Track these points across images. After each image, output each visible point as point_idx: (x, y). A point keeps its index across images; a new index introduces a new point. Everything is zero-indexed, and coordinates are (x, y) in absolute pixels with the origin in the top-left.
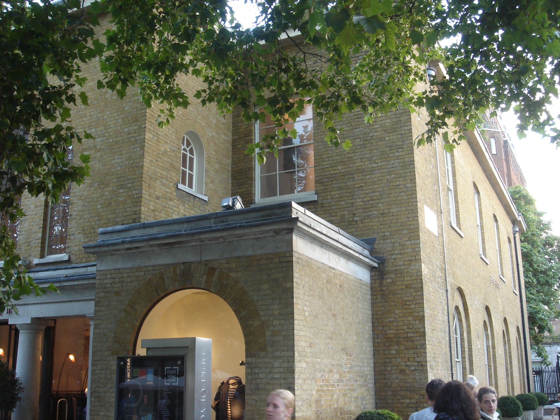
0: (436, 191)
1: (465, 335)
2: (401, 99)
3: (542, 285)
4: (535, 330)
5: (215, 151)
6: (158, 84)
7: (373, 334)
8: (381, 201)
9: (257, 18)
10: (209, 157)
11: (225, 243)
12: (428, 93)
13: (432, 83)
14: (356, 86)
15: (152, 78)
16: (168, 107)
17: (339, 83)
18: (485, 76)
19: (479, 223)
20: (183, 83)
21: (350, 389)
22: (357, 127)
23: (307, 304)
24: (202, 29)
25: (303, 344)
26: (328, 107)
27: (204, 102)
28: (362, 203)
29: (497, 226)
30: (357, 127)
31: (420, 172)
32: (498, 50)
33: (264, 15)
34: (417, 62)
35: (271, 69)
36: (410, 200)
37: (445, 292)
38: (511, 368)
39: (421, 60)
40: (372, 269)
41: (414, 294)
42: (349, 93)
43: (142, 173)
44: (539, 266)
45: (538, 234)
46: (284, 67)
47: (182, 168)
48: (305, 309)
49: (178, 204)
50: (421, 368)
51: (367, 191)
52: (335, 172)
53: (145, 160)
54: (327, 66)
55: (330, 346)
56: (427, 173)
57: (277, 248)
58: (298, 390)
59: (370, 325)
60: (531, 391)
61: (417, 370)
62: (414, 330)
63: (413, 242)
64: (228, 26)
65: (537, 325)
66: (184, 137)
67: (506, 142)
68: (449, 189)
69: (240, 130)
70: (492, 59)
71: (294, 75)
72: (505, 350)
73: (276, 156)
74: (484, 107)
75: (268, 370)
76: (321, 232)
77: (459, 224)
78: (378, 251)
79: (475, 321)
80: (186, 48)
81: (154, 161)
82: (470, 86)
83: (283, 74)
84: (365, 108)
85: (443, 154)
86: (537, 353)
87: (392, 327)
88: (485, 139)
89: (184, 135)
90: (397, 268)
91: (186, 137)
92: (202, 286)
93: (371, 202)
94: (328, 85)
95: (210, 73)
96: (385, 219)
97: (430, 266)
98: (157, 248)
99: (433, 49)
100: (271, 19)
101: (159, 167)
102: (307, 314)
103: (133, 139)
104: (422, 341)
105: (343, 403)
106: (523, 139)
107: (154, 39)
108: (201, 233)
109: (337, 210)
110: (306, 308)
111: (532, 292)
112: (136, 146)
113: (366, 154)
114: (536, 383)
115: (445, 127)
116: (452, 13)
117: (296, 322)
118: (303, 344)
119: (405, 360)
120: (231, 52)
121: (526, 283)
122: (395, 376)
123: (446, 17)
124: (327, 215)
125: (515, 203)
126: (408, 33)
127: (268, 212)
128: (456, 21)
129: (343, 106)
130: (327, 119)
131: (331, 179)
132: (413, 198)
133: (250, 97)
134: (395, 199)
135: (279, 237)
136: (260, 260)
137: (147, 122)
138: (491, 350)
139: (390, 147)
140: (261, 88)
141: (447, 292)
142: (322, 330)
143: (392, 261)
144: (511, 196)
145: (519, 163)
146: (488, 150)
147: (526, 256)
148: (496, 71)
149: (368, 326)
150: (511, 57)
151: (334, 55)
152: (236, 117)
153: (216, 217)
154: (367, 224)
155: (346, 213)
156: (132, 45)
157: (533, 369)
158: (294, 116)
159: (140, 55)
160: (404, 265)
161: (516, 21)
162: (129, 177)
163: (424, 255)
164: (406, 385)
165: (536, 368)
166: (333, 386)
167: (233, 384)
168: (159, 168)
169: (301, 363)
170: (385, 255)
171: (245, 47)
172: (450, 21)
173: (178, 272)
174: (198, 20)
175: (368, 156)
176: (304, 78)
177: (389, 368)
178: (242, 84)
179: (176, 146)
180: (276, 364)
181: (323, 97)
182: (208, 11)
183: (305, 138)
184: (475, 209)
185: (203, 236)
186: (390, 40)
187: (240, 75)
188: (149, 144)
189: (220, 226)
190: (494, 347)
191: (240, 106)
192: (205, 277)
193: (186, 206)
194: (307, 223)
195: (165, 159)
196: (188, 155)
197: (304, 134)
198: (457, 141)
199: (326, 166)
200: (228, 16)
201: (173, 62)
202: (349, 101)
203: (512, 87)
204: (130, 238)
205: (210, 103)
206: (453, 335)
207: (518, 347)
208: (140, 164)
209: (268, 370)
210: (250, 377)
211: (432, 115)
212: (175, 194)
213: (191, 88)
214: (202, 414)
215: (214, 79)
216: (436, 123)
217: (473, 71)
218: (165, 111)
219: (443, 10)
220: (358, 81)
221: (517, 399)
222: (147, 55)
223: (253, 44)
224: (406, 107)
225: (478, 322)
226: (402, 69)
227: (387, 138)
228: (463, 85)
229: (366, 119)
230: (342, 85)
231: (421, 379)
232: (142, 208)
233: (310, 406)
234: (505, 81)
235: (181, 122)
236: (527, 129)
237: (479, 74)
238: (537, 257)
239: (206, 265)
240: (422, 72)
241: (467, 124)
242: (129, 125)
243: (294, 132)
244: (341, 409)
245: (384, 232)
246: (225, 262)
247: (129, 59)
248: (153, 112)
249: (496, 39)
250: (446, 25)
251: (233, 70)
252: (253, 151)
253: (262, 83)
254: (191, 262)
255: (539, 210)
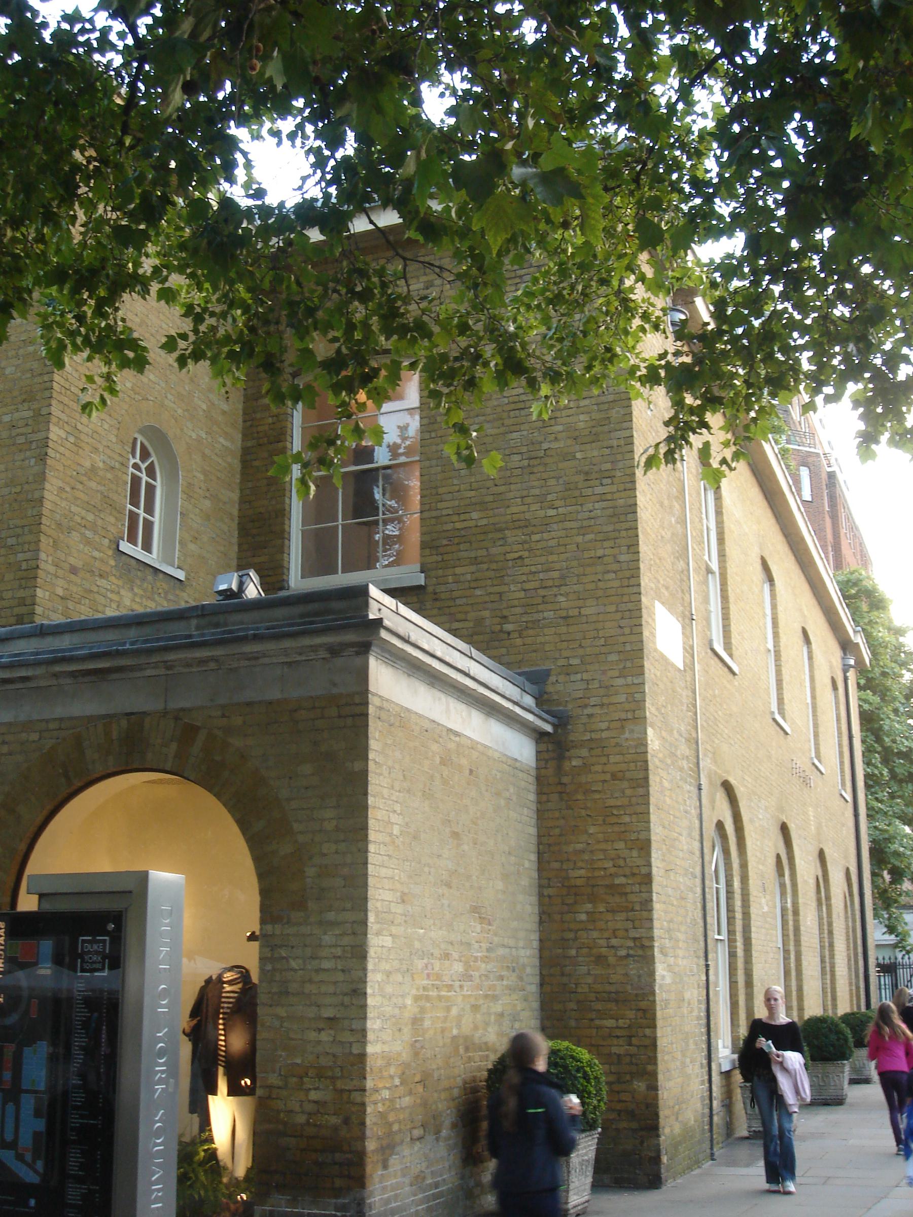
0: (682, 572)
1: (737, 884)
2: (612, 370)
3: (901, 781)
4: (883, 877)
5: (205, 473)
6: (80, 318)
7: (540, 878)
8: (564, 589)
9: (304, 179)
10: (190, 485)
11: (220, 671)
12: (670, 357)
13: (679, 336)
14: (514, 337)
15: (68, 304)
16: (105, 370)
17: (479, 327)
18: (793, 325)
19: (770, 645)
20: (137, 320)
21: (486, 996)
22: (513, 428)
23: (398, 808)
24: (181, 200)
25: (387, 896)
26: (453, 378)
27: (182, 361)
28: (522, 594)
29: (810, 653)
30: (513, 428)
31: (649, 531)
32: (821, 271)
33: (319, 173)
34: (648, 289)
35: (330, 292)
36: (626, 590)
37: (696, 791)
38: (832, 956)
39: (656, 286)
40: (540, 736)
41: (628, 792)
42: (500, 350)
43: (40, 515)
44: (894, 741)
45: (894, 673)
46: (359, 289)
47: (129, 506)
48: (393, 820)
49: (118, 586)
50: (640, 952)
51: (533, 569)
52: (465, 524)
53: (47, 486)
54: (450, 292)
55: (446, 902)
56: (664, 534)
57: (335, 685)
58: (373, 995)
59: (534, 857)
60: (873, 1007)
61: (632, 956)
62: (627, 871)
63: (629, 679)
64: (237, 193)
65: (889, 866)
66: (135, 439)
67: (832, 476)
68: (709, 571)
69: (260, 428)
70: (808, 289)
71: (380, 305)
72: (820, 918)
73: (338, 482)
74: (789, 390)
75: (308, 951)
76: (431, 651)
77: (728, 646)
78: (555, 697)
79: (758, 854)
80: (145, 236)
81: (68, 489)
82: (760, 345)
83: (356, 303)
84: (533, 384)
85: (699, 494)
86: (886, 926)
87: (580, 864)
88: (788, 467)
89: (136, 435)
90: (594, 736)
91: (140, 438)
92: (168, 768)
93: (542, 592)
94: (455, 331)
95: (198, 297)
96: (572, 629)
97: (664, 734)
98: (69, 681)
99: (682, 265)
100: (335, 181)
101: (79, 502)
102: (396, 830)
103: (21, 440)
104: (644, 895)
105: (472, 1026)
106: (870, 462)
107: (74, 218)
108: (166, 649)
109: (468, 608)
110: (394, 818)
111: (880, 795)
112: (28, 453)
113: (533, 487)
114: (883, 991)
115: (704, 431)
116: (725, 188)
117: (372, 848)
118: (387, 896)
119: (606, 935)
120: (244, 252)
121: (867, 776)
122: (584, 969)
123: (714, 195)
124: (444, 618)
125: (847, 605)
126: (630, 227)
127: (315, 606)
128: (734, 204)
129: (485, 380)
130: (452, 405)
131: (456, 540)
132: (633, 586)
133: (283, 350)
134: (592, 586)
135: (339, 662)
136: (296, 710)
137: (54, 402)
138: (790, 917)
139: (587, 473)
140: (308, 332)
141: (700, 789)
142: (429, 865)
143: (584, 720)
144: (841, 590)
145: (857, 522)
146: (794, 490)
147: (869, 720)
148: (816, 315)
149: (530, 861)
150: (848, 286)
151: (469, 268)
152: (251, 399)
153: (203, 616)
154: (528, 641)
155: (486, 614)
156: (24, 230)
157: (877, 959)
158: (380, 396)
159: (42, 251)
160: (608, 729)
161: (859, 207)
162: (11, 522)
163: (653, 710)
164: (608, 988)
165: (884, 959)
166: (450, 987)
167: (230, 983)
168: (78, 506)
169: (381, 937)
170: (570, 707)
171: (274, 240)
172: (723, 205)
173: (115, 735)
174: (174, 179)
175: (537, 492)
176: (403, 314)
177: (573, 952)
178: (267, 322)
179: (117, 457)
180: (327, 939)
181: (444, 358)
182: (196, 157)
183: (401, 451)
184: (764, 615)
185: (172, 656)
186: (593, 222)
187: (262, 303)
188: (57, 451)
189: (210, 634)
190: (796, 913)
191: (261, 369)
192: (174, 746)
193: (136, 590)
194: (401, 631)
195: (93, 485)
196: (145, 478)
197: (399, 441)
198: (730, 462)
199: (445, 512)
200: (240, 173)
201: (117, 269)
202: (501, 367)
203: (849, 350)
204: (10, 656)
205: (196, 363)
206: (711, 884)
207: (846, 912)
208: (37, 495)
209: (308, 951)
210: (269, 967)
211: (678, 404)
212: (112, 563)
213: (153, 332)
214: (160, 1040)
215: (205, 310)
216: (685, 423)
217: (767, 313)
218: (97, 378)
219: (706, 179)
220: (520, 327)
221: (843, 1022)
222: (58, 251)
223: (292, 236)
224: (623, 387)
225: (765, 857)
226: (616, 304)
227: (579, 455)
228: (745, 342)
229: (535, 409)
230: (485, 331)
231: (639, 976)
232: (39, 592)
233: (400, 1030)
234: (835, 338)
235: (131, 405)
236: (877, 442)
237: (780, 320)
238: (890, 723)
239: (177, 718)
240: (659, 313)
241: (753, 427)
242: (13, 407)
243: (379, 433)
244: (466, 1038)
245: (568, 658)
246: (219, 713)
247: (16, 257)
248: (67, 380)
249: (817, 248)
250: (713, 213)
251: (249, 290)
252: (287, 469)
253: (310, 320)
254: (144, 713)
255: (897, 623)
